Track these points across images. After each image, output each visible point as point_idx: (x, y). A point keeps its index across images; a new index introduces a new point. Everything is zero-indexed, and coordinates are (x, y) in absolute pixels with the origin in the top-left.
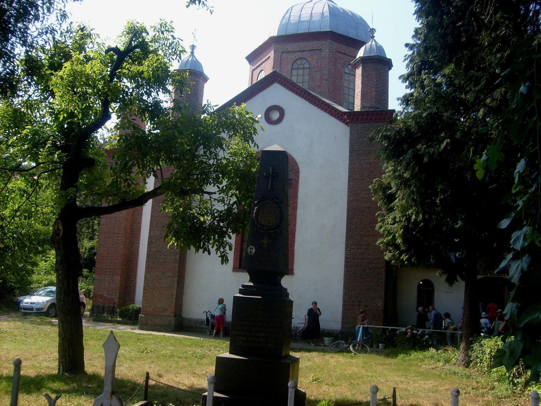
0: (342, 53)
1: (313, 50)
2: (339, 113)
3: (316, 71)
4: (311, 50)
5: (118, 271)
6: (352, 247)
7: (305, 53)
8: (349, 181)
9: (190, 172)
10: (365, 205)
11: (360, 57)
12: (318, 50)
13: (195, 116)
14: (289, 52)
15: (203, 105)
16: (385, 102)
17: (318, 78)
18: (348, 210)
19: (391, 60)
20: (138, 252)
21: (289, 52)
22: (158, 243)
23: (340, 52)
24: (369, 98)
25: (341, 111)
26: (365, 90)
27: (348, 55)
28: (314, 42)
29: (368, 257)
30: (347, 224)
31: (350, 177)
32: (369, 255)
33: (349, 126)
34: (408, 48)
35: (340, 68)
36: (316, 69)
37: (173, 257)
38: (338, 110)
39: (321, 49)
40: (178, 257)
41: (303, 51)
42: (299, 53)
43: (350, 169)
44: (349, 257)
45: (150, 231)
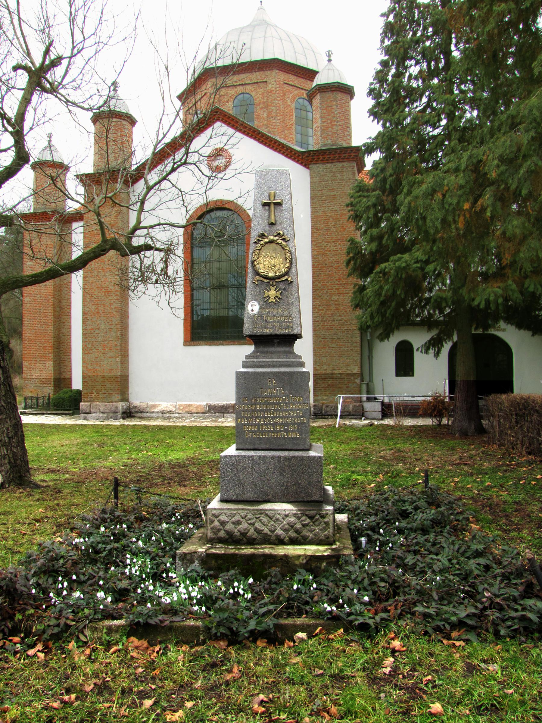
0: (291, 85)
1: (257, 83)
2: (295, 154)
3: (261, 108)
4: (255, 83)
5: (50, 355)
6: (321, 308)
7: (248, 87)
8: (313, 233)
9: (212, 600)
10: (331, 259)
11: (317, 85)
12: (263, 82)
13: (85, 531)
14: (229, 86)
15: (10, 638)
16: (349, 138)
17: (265, 115)
18: (313, 266)
19: (353, 87)
20: (70, 332)
21: (229, 86)
22: (94, 319)
23: (288, 84)
24: (330, 133)
25: (297, 151)
26: (325, 124)
27: (298, 87)
28: (258, 73)
29: (340, 318)
30: (313, 282)
31: (313, 227)
32: (340, 316)
33: (308, 168)
34: (379, 67)
35: (290, 103)
36: (261, 106)
37: (113, 334)
38: (295, 150)
39: (266, 82)
40: (119, 333)
41: (246, 84)
42: (241, 87)
43: (312, 219)
44: (317, 320)
45: (84, 306)
